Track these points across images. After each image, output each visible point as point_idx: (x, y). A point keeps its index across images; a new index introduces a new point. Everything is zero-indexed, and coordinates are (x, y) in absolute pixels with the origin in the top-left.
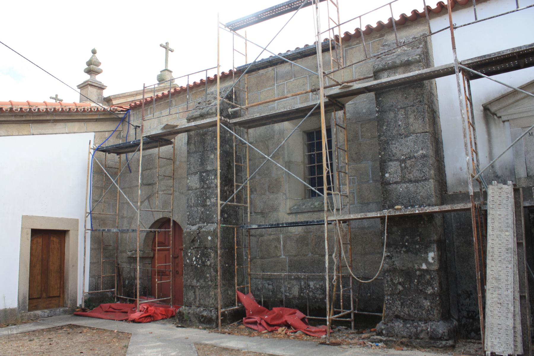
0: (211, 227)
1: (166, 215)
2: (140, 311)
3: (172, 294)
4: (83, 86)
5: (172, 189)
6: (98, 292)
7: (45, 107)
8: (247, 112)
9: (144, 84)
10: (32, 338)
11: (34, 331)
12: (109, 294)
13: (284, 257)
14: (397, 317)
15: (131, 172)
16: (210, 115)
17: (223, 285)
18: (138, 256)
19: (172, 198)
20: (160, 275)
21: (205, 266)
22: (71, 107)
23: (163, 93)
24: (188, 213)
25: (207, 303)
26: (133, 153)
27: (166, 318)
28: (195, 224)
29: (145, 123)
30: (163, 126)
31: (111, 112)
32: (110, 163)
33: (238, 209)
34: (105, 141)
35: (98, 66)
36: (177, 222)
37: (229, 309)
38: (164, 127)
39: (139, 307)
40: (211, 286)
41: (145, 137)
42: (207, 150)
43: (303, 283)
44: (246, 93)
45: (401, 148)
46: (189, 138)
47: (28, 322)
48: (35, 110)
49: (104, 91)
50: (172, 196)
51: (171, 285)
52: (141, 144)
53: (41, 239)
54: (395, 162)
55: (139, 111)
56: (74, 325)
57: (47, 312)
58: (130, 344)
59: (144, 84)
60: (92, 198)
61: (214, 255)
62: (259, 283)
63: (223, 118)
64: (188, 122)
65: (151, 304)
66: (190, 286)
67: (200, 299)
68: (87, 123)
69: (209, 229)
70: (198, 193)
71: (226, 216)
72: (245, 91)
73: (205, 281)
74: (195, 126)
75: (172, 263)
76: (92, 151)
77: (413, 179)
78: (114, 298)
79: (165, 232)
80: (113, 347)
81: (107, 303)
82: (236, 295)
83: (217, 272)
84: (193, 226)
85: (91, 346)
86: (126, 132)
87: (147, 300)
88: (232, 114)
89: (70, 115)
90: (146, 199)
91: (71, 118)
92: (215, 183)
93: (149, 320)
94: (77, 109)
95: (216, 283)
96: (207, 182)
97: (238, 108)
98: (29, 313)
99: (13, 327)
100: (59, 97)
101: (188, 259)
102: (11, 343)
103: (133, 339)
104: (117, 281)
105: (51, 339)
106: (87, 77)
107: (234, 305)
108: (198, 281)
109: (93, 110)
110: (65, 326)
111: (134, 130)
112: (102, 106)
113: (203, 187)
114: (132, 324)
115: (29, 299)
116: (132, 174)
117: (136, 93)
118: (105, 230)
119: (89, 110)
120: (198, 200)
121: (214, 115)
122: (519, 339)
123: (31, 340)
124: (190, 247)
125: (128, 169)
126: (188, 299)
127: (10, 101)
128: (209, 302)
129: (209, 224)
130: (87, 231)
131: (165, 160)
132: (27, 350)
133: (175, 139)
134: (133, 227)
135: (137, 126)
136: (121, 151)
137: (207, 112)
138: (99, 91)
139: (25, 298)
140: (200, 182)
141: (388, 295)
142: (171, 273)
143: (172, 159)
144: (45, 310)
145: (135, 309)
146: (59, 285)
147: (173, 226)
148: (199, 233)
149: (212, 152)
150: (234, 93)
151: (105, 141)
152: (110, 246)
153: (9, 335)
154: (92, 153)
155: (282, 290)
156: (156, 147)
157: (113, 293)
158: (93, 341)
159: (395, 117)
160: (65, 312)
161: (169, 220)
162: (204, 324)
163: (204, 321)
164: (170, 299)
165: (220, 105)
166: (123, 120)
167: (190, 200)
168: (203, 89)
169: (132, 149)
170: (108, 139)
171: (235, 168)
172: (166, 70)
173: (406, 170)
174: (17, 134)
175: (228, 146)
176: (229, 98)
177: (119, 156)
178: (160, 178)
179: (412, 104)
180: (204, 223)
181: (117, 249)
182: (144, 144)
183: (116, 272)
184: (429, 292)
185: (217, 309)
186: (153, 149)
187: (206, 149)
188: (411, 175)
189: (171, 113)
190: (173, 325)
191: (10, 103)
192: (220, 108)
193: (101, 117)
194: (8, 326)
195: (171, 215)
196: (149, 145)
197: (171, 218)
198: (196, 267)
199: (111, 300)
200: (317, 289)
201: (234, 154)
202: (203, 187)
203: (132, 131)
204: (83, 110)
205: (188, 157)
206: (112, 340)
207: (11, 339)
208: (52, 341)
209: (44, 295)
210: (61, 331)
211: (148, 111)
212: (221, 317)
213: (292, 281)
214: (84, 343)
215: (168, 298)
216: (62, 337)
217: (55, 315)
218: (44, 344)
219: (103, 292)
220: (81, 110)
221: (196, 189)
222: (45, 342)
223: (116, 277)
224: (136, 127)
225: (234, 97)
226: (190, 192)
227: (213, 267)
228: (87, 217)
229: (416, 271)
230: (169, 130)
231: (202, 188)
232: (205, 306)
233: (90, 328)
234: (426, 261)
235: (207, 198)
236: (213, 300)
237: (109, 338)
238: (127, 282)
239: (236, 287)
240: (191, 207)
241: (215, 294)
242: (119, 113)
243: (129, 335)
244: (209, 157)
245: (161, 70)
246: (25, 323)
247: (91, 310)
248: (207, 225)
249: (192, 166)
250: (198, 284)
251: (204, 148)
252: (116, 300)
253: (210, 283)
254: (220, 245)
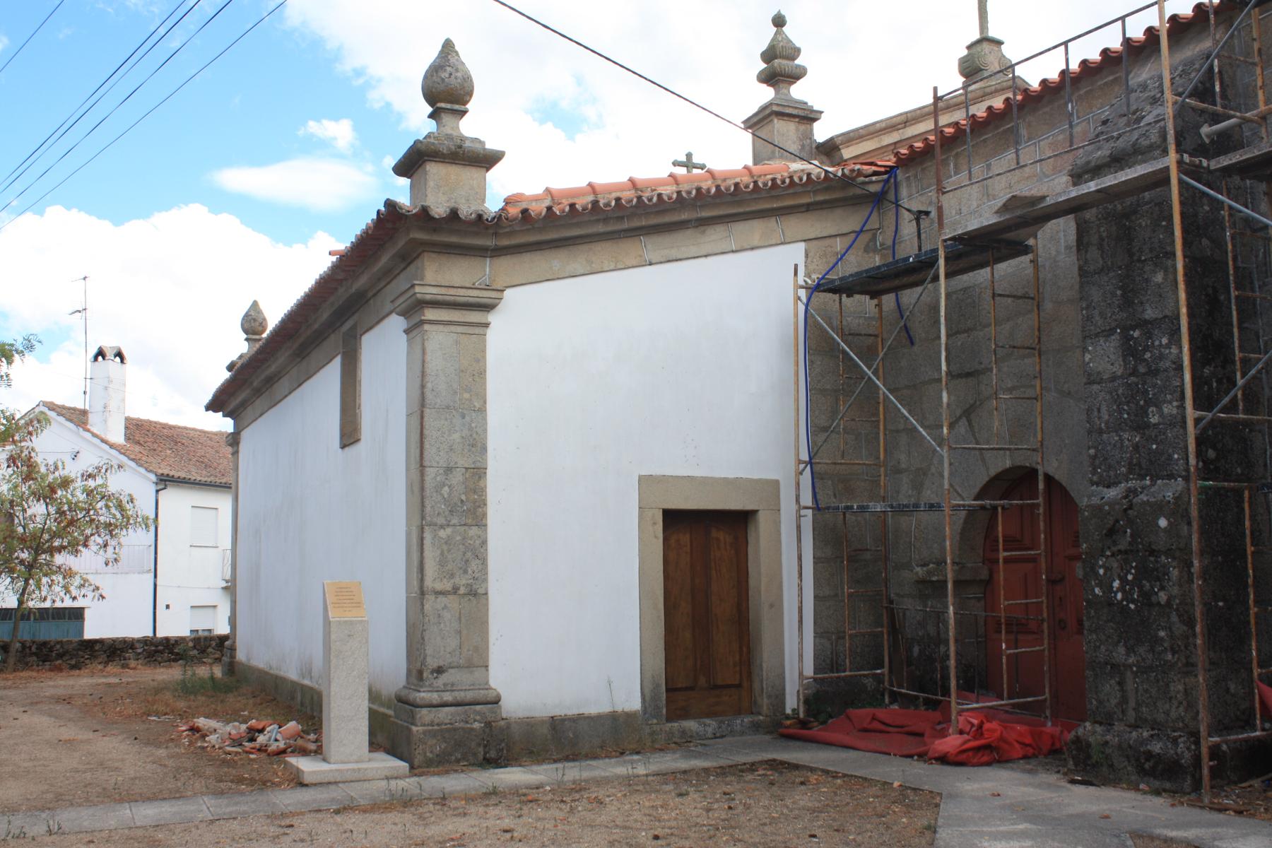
0: (1169, 490)
1: (1024, 460)
2: (961, 732)
3: (1050, 687)
4: (758, 123)
5: (1038, 382)
6: (838, 677)
7: (674, 188)
8: (1263, 130)
9: (935, 89)
10: (684, 788)
11: (685, 772)
12: (869, 682)
15: (912, 343)
16: (1142, 154)
17: (1212, 663)
18: (950, 576)
19: (1039, 410)
20: (1012, 632)
21: (1151, 605)
22: (738, 180)
23: (990, 108)
24: (1092, 451)
25: (1161, 717)
26: (919, 289)
27: (1035, 756)
28: (1116, 484)
29: (948, 202)
30: (999, 203)
31: (847, 181)
32: (852, 322)
33: (1251, 431)
34: (837, 263)
35: (794, 59)
36: (1057, 477)
37: (1232, 737)
38: (1004, 205)
39: (957, 720)
41: (950, 239)
42: (1139, 260)
44: (1258, 70)
46: (1082, 231)
47: (668, 749)
48: (650, 200)
49: (816, 125)
50: (1039, 404)
51: (1046, 659)
52: (942, 262)
53: (688, 536)
55: (923, 170)
56: (782, 763)
57: (712, 724)
58: (940, 821)
59: (935, 89)
60: (812, 421)
61: (1180, 572)
63: (1186, 158)
64: (1075, 184)
65: (989, 714)
66: (1106, 664)
67: (1138, 704)
68: (783, 218)
69: (1160, 497)
70: (1120, 391)
71: (1211, 454)
72: (1255, 64)
73: (1152, 650)
74: (1098, 191)
75: (1047, 597)
76: (803, 293)
78: (883, 695)
79: (1022, 506)
80: (895, 828)
81: (864, 707)
82: (1257, 697)
83: (1190, 623)
84: (1108, 487)
85: (834, 820)
86: (890, 232)
87: (977, 702)
88: (1212, 141)
89: (740, 203)
90: (960, 417)
91: (741, 210)
92: (1172, 357)
93: (985, 758)
94: (755, 182)
95: (1187, 657)
96: (1148, 355)
97: (1233, 121)
98: (669, 725)
99: (636, 757)
100: (695, 160)
101: (1097, 585)
102: (637, 798)
103: (947, 809)
104: (889, 648)
105: (729, 794)
106: (766, 94)
107: (1248, 724)
108: (1130, 650)
109: (796, 179)
110: (761, 762)
111: (914, 223)
112: (815, 168)
113: (1134, 373)
114: (938, 768)
115: (668, 690)
116: (916, 348)
117: (903, 118)
118: (852, 507)
119: (787, 181)
120: (1120, 412)
121: (1157, 153)
123: (681, 795)
124: (1103, 551)
125: (904, 334)
126: (1100, 702)
127: (590, 185)
128: (1167, 713)
129: (1159, 482)
130: (803, 512)
131: (1010, 300)
132: (676, 819)
133: (1036, 237)
134: (929, 495)
135: (920, 212)
136: (881, 287)
137: (1134, 145)
138: (802, 127)
139: (658, 686)
140: (1124, 357)
142: (1045, 625)
143: (1031, 297)
144: (708, 721)
145: (944, 725)
146: (737, 658)
147: (1044, 489)
148: (1131, 507)
149: (1156, 265)
150: (1217, 77)
151: (837, 263)
152: (867, 550)
153: (628, 777)
154: (804, 300)
156: (982, 266)
157: (879, 679)
158: (838, 806)
160: (756, 727)
161: (1033, 472)
162: (1155, 778)
164: (1046, 700)
165: (1175, 117)
166: (878, 200)
167: (1096, 413)
168: (1111, 78)
169: (912, 279)
170: (843, 256)
171: (1234, 307)
172: (985, 39)
174: (612, 267)
175: (1205, 241)
176: (1202, 92)
177: (875, 301)
178: (1000, 352)
180: (1143, 478)
181: (886, 559)
182: (947, 259)
183: (885, 623)
185: (1195, 736)
186: (971, 274)
187: (1135, 258)
189: (1022, 164)
190: (1058, 776)
191: (590, 189)
192: (1175, 128)
193: (820, 198)
194: (622, 754)
195: (1040, 460)
196: (963, 263)
197: (1039, 467)
198: (1124, 610)
199: (875, 698)
201: (1231, 263)
202: (1134, 373)
203: (908, 228)
204: (770, 183)
205: (1082, 285)
206: (889, 808)
207: (636, 788)
208: (733, 799)
209: (702, 681)
210: (749, 777)
211: (949, 165)
212: (1211, 760)
214: (814, 811)
215: (1040, 698)
216: (756, 793)
217: (732, 733)
218: (716, 806)
219: (851, 676)
220: (765, 184)
221: (1114, 378)
222: (717, 801)
223: (885, 636)
224: (920, 215)
225: (1217, 88)
226: (1096, 387)
227: (1177, 610)
228: (801, 473)
230: (1019, 212)
231: (1131, 375)
232: (1155, 725)
233: (826, 772)
235: (1149, 402)
236: (1181, 709)
237: (880, 802)
238: (916, 650)
239: (1256, 671)
240: (1101, 432)
241: (1186, 690)
242: (867, 179)
243: (933, 798)
244: (1147, 281)
245: (969, 43)
246: (661, 750)
247: (822, 723)
248: (1153, 485)
249: (1096, 312)
251: (1131, 255)
252: (887, 701)
253: (1169, 657)
254: (1200, 541)
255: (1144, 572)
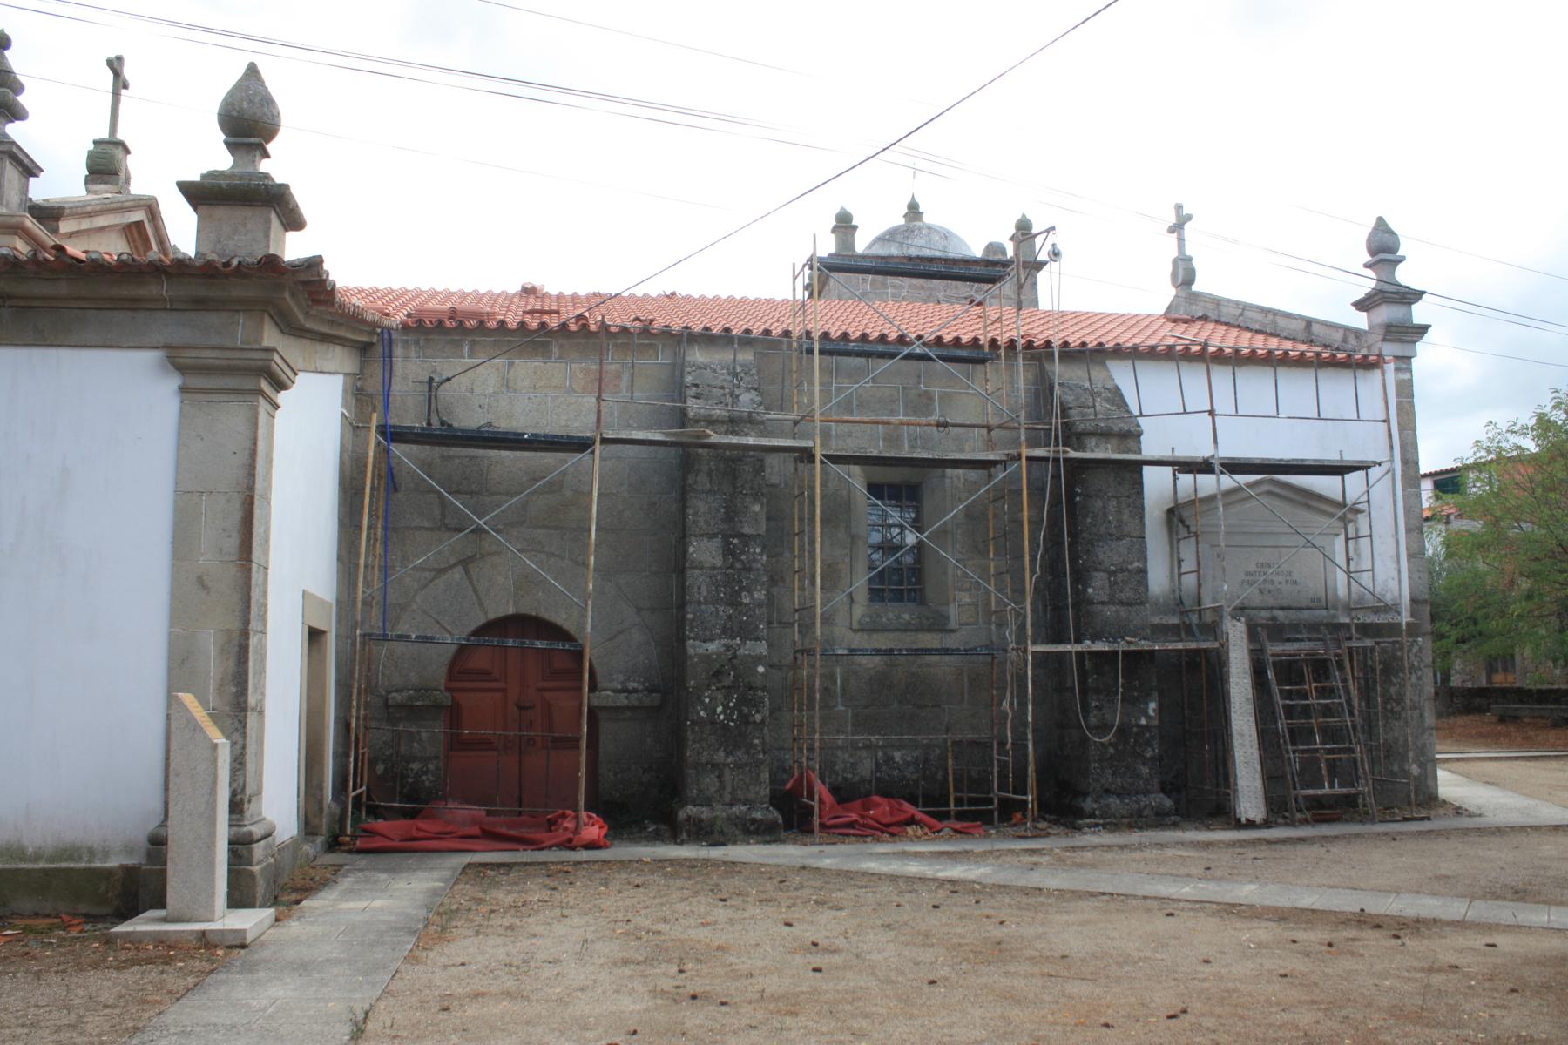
13: (843, 708)
14: (1107, 791)
25: (751, 796)
40: (762, 762)
43: (880, 754)
45: (1110, 554)
54: (1102, 574)
62: (787, 757)
70: (719, 577)
77: (1125, 601)
90: (455, 565)
96: (743, 557)
101: (702, 710)
108: (728, 754)
113: (732, 567)
116: (400, 495)
122: (1135, 837)
126: (700, 791)
128: (757, 793)
140: (724, 556)
141: (1095, 762)
149: (755, 499)
155: (837, 768)
159: (1104, 507)
163: (758, 829)
167: (696, 590)
168: (647, 342)
173: (1115, 587)
179: (1127, 493)
180: (733, 638)
184: (1148, 755)
188: (1122, 595)
198: (725, 727)
200: (908, 764)
213: (859, 752)
221: (713, 568)
229: (1133, 726)
234: (1146, 714)
235: (742, 589)
249: (701, 520)
250: (730, 760)
251: (735, 488)
253: (761, 756)
255: (743, 701)
